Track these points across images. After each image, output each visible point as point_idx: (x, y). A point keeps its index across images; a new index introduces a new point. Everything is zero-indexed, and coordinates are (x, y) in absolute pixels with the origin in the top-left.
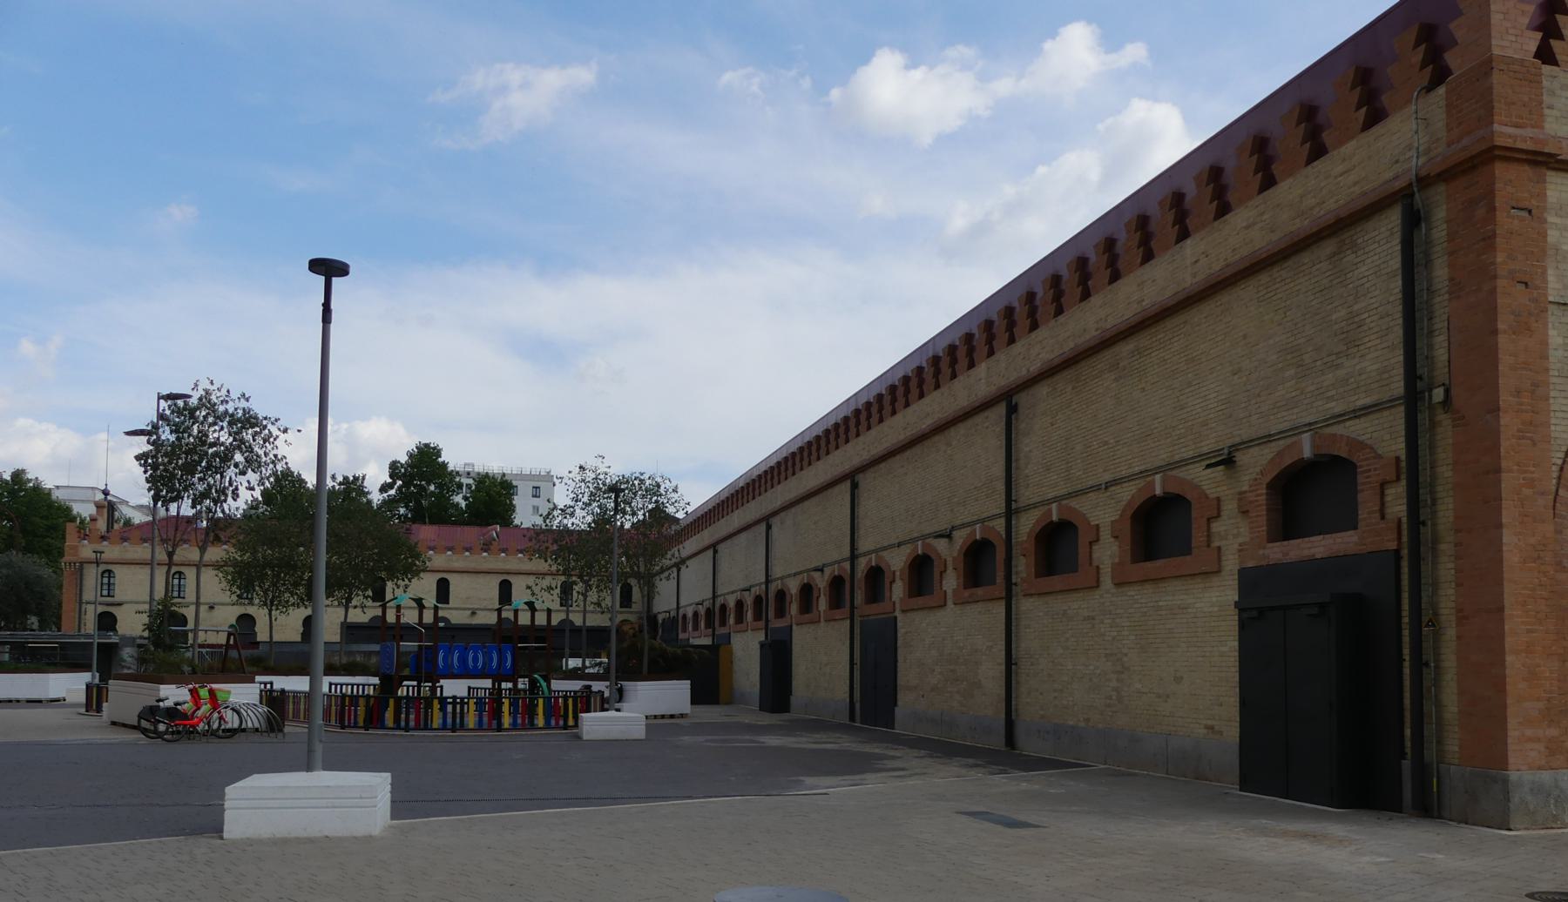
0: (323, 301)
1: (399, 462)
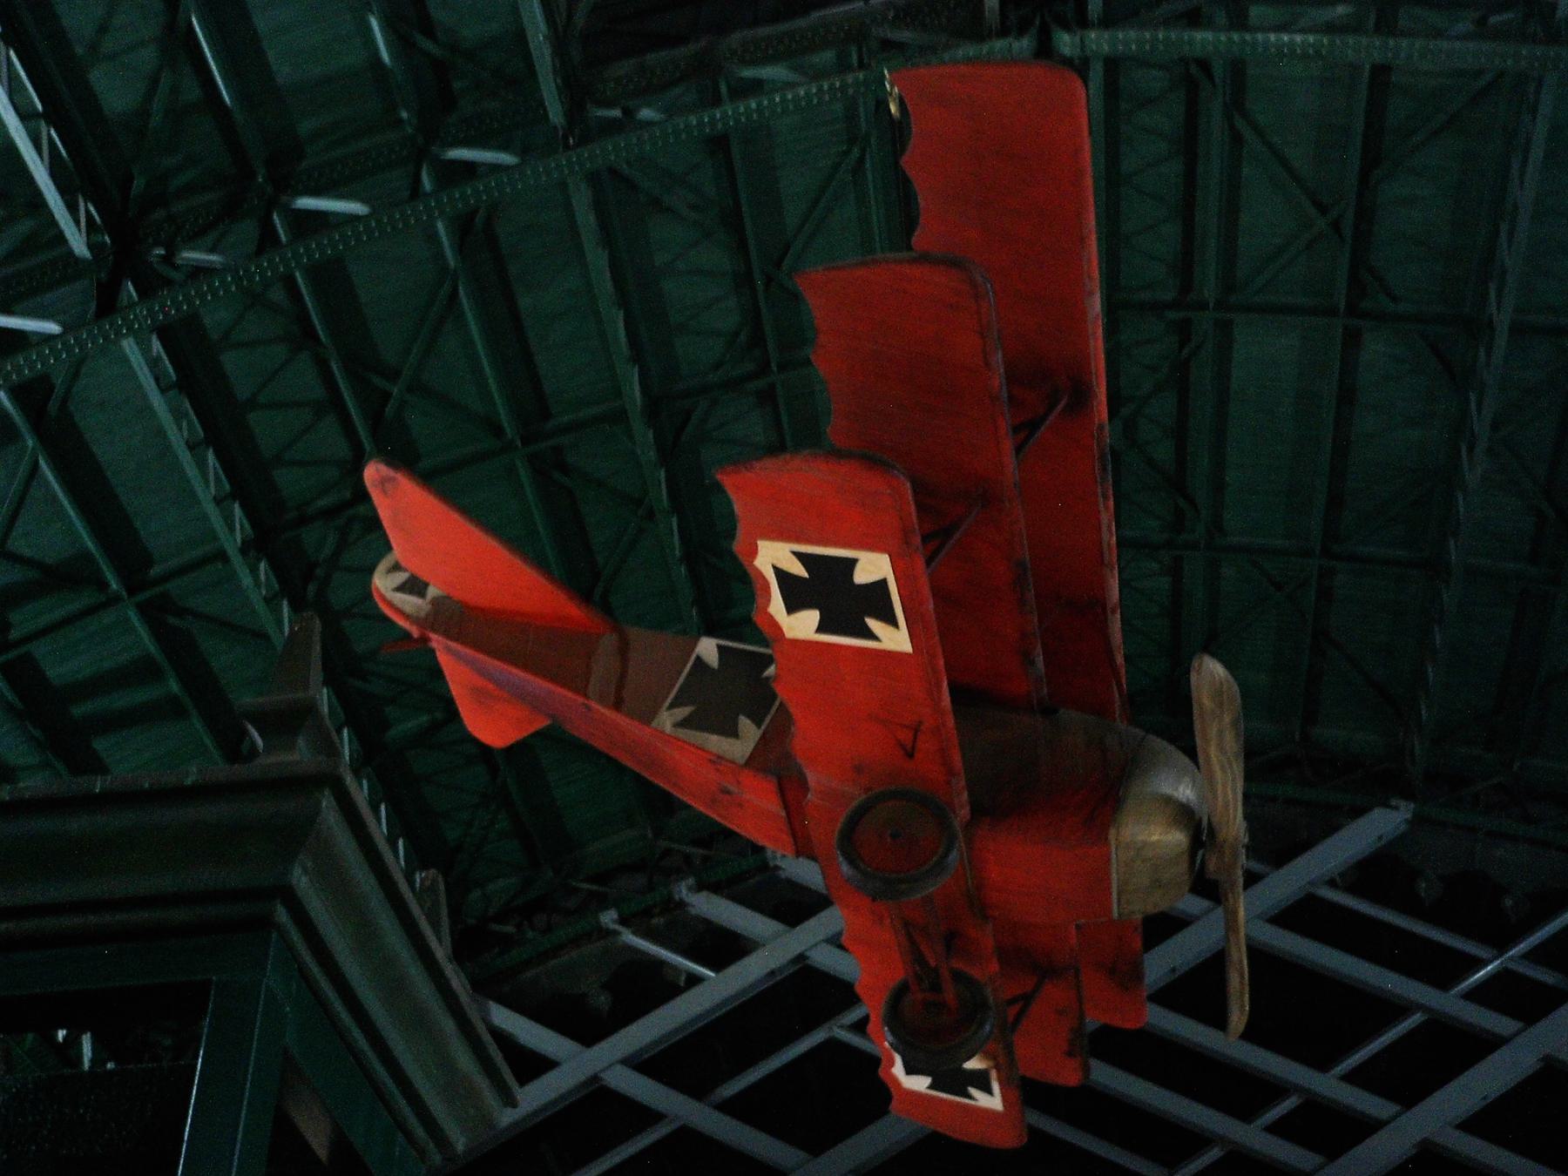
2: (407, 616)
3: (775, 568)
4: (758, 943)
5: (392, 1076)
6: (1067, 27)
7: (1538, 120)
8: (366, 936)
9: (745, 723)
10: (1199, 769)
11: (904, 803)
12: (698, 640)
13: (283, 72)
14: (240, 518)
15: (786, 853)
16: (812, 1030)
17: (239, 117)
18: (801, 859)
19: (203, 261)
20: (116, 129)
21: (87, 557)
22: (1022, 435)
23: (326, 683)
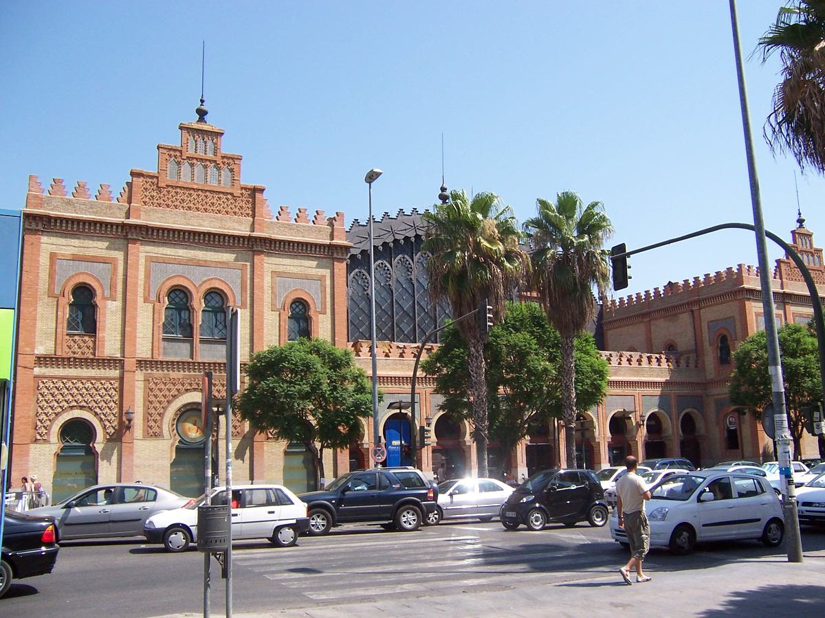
0: (784, 253)
1: (512, 211)
2: (545, 305)
3: (292, 503)
4: (36, 590)
5: (94, 542)
6: (317, 264)
7: (535, 341)
8: (545, 559)
9: (737, 271)
10: (633, 606)
11: (644, 536)
12: (97, 493)
13: (122, 253)
14: (674, 473)
15: (603, 435)
16: (646, 448)
17: (546, 509)
18: (429, 203)
19: (76, 452)
20: (490, 334)
21: (101, 458)
22: (115, 458)
23: (207, 477)
